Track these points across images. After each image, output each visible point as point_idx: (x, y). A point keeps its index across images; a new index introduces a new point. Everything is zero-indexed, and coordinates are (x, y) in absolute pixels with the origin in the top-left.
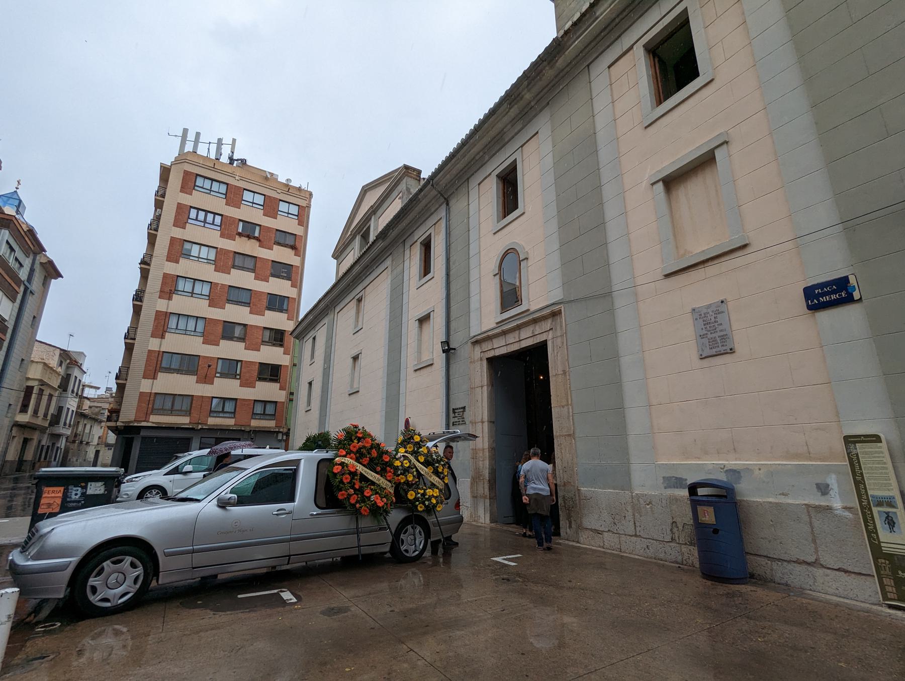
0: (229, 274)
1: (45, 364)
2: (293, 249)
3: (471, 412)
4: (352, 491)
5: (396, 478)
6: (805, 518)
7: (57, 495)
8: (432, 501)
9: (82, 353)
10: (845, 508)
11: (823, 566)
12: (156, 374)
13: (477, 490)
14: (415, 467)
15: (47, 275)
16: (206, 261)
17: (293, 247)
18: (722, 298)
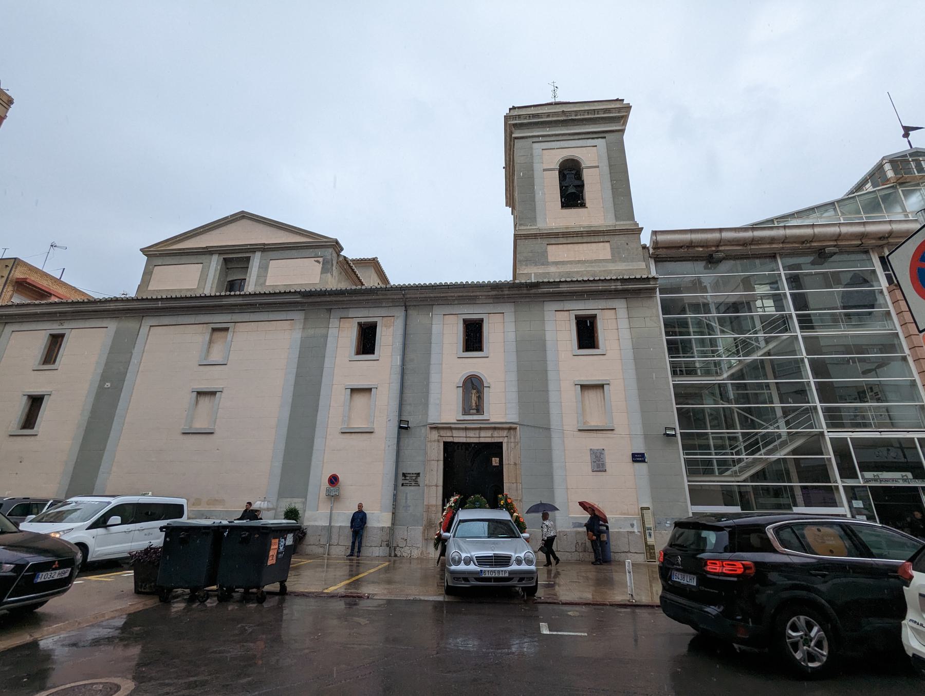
6: (627, 536)
10: (639, 532)
11: (631, 552)
18: (22, 463)
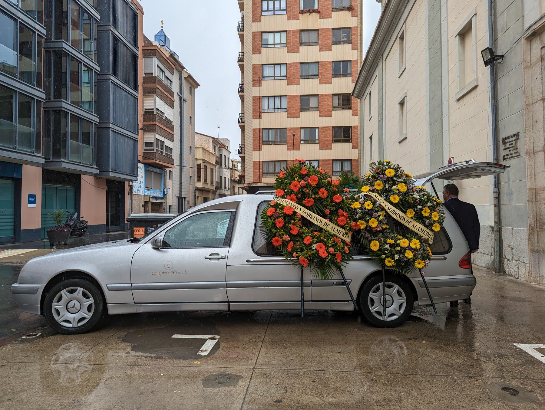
0: (298, 52)
1: (203, 148)
2: (349, 10)
3: (528, 139)
4: (287, 237)
5: (353, 223)
7: (141, 233)
8: (406, 255)
9: (227, 139)
12: (260, 147)
13: (538, 242)
14: (383, 209)
15: (191, 86)
16: (279, 46)
17: (350, 9)
